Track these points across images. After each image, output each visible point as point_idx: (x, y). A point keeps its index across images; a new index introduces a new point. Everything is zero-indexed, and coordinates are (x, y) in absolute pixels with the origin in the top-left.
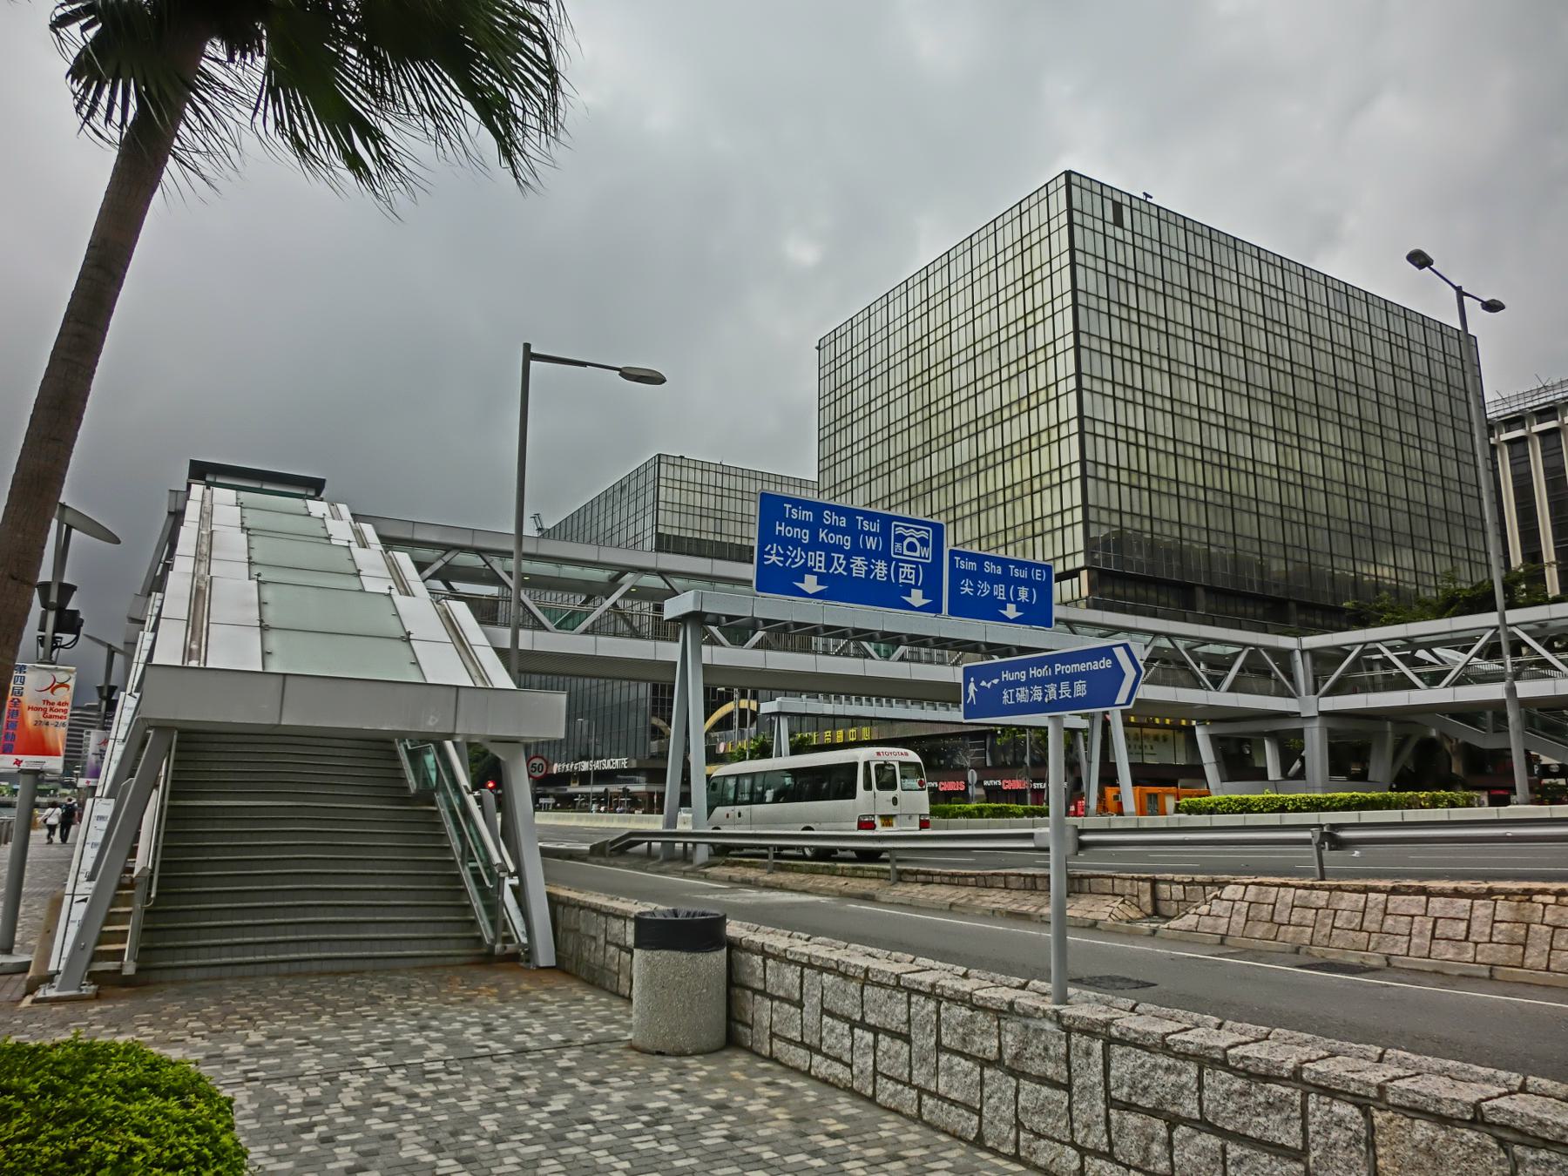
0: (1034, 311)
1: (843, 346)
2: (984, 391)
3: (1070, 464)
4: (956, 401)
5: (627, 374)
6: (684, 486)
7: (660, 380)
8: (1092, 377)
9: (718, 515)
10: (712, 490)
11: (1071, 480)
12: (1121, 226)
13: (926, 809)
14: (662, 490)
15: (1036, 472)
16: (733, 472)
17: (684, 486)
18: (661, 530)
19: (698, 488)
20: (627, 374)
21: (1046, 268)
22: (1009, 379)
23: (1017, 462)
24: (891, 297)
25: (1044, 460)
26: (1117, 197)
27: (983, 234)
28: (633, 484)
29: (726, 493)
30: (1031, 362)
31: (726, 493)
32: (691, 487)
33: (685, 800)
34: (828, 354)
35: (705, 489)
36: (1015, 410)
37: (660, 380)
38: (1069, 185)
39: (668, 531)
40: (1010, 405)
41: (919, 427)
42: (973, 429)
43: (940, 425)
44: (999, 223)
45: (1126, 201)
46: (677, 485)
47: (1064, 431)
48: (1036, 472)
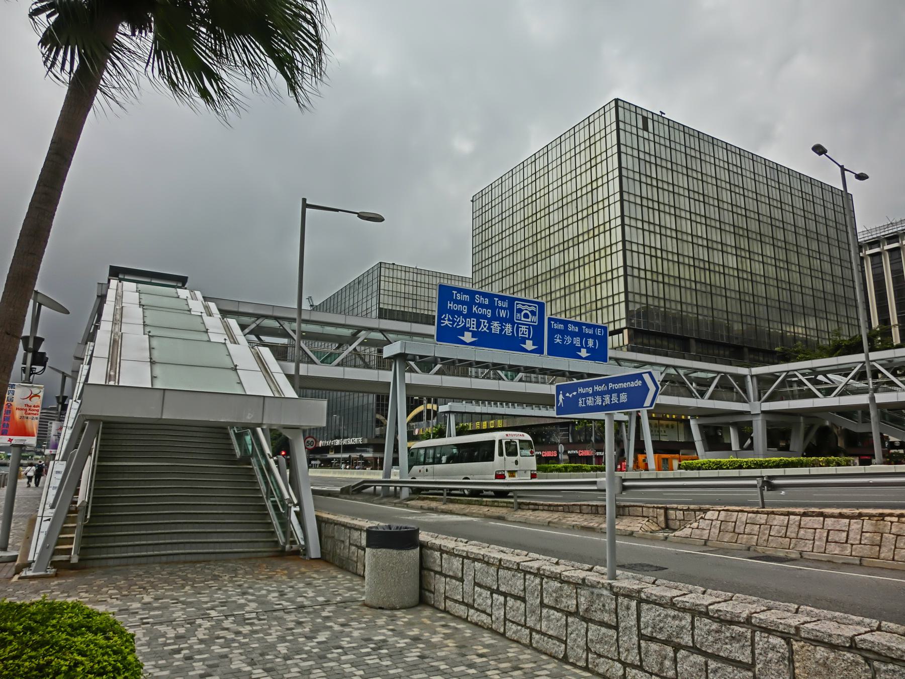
0: (597, 179)
1: (486, 200)
2: (568, 226)
3: (618, 268)
4: (552, 231)
5: (362, 216)
6: (395, 280)
7: (381, 219)
8: (630, 218)
9: (415, 297)
10: (411, 283)
11: (618, 277)
12: (647, 130)
13: (534, 467)
14: (382, 283)
15: (598, 272)
16: (423, 272)
17: (395, 280)
18: (381, 306)
19: (403, 282)
20: (362, 216)
21: (604, 155)
22: (583, 219)
23: (587, 267)
24: (514, 171)
25: (602, 266)
26: (645, 114)
27: (567, 135)
28: (365, 280)
29: (419, 284)
30: (595, 209)
31: (419, 284)
32: (399, 281)
33: (396, 462)
34: (478, 205)
35: (407, 282)
36: (586, 237)
37: (381, 219)
38: (617, 107)
39: (386, 307)
40: (583, 234)
41: (531, 247)
42: (561, 248)
43: (542, 245)
44: (577, 129)
45: (650, 116)
46: (391, 280)
47: (614, 249)
48: (598, 272)
